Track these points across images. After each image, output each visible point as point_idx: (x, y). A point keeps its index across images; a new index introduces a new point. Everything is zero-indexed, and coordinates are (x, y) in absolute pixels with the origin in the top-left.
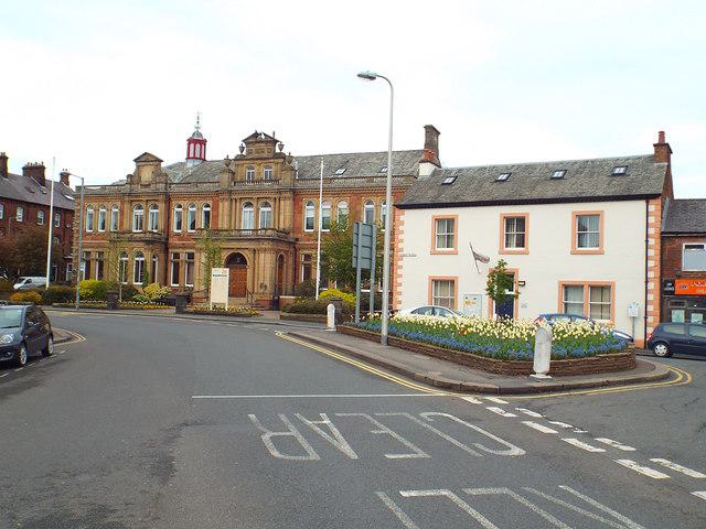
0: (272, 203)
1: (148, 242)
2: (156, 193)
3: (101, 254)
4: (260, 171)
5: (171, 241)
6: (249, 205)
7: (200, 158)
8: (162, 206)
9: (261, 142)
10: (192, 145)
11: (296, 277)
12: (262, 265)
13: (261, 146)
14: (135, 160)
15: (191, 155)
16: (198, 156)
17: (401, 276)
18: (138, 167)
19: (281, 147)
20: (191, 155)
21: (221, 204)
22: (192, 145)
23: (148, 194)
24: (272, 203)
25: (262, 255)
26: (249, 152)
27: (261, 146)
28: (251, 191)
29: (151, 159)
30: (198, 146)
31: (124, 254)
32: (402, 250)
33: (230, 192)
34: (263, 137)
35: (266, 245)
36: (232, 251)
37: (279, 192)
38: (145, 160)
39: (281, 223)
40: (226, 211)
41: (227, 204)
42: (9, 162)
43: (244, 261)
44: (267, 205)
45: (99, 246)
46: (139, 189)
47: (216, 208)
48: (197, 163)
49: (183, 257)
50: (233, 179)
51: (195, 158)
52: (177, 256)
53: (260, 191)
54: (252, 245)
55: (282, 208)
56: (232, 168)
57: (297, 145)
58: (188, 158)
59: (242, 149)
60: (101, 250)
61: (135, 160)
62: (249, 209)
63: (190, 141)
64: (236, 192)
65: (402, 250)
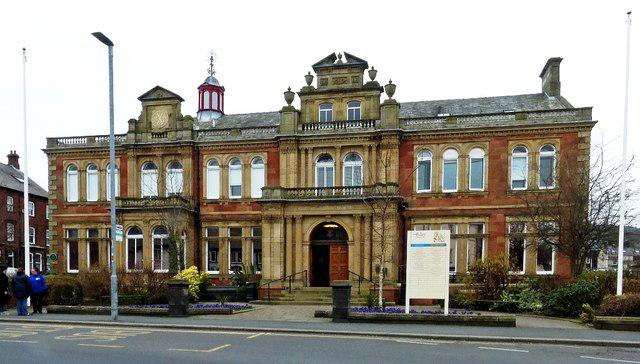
2: (178, 145)
3: (93, 232)
4: (343, 108)
5: (204, 211)
6: (150, 166)
7: (218, 111)
8: (187, 162)
9: (340, 67)
10: (207, 94)
13: (341, 76)
14: (142, 98)
15: (206, 106)
16: (215, 107)
18: (146, 109)
19: (373, 73)
20: (206, 106)
22: (207, 94)
23: (166, 146)
26: (323, 82)
27: (341, 76)
28: (329, 138)
29: (165, 96)
30: (215, 94)
33: (298, 140)
34: (344, 60)
36: (321, 221)
37: (377, 137)
38: (156, 97)
41: (293, 156)
44: (353, 157)
45: (88, 221)
46: (147, 139)
48: (216, 116)
49: (224, 232)
50: (299, 122)
51: (210, 109)
52: (214, 232)
53: (345, 136)
54: (359, 210)
57: (417, 78)
58: (202, 110)
59: (309, 78)
60: (93, 226)
61: (142, 98)
62: (93, 171)
63: (203, 89)
64: (311, 139)
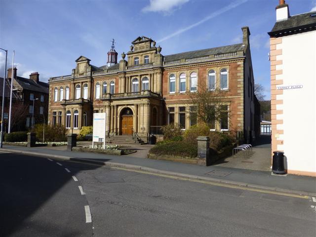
0: (148, 77)
1: (62, 105)
5: (94, 104)
11: (30, 120)
12: (142, 115)
15: (110, 61)
17: (281, 112)
21: (120, 80)
24: (148, 77)
25: (142, 108)
31: (69, 112)
32: (281, 82)
35: (145, 101)
36: (124, 107)
39: (155, 88)
40: (123, 85)
41: (123, 80)
42: (39, 76)
43: (131, 113)
46: (77, 76)
47: (117, 84)
55: (155, 79)
56: (126, 59)
65: (281, 82)
